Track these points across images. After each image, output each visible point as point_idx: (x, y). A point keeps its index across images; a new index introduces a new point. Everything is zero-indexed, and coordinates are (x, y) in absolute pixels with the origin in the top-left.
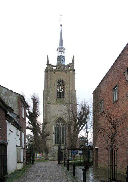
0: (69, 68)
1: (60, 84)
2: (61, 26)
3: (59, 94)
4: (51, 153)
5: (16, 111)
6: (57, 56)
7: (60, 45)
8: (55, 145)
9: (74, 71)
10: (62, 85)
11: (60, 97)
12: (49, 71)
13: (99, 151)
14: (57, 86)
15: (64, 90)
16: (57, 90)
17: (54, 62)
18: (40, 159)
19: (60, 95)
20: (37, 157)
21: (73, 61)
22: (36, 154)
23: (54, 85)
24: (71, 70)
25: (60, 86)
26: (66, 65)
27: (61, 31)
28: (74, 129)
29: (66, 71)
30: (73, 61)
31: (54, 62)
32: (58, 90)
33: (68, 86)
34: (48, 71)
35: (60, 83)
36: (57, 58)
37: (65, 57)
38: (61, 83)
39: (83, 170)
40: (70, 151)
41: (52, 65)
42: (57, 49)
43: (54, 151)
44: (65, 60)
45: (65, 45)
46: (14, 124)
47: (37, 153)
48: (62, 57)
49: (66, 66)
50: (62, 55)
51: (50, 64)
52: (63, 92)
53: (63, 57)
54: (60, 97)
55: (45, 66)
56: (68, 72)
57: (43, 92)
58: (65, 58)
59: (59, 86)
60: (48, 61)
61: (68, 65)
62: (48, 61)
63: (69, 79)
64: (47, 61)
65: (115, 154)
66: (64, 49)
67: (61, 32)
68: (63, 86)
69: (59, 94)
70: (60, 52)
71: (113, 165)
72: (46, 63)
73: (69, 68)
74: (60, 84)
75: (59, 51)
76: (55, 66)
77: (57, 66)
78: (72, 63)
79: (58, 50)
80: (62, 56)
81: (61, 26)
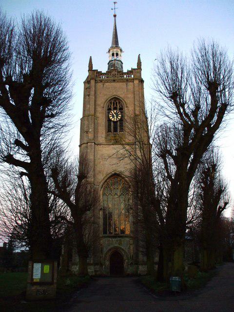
0: (132, 76)
2: (115, 16)
3: (112, 124)
7: (113, 44)
8: (104, 235)
9: (142, 81)
11: (115, 130)
12: (93, 82)
17: (103, 68)
18: (45, 288)
19: (115, 129)
20: (32, 279)
21: (139, 64)
24: (136, 79)
25: (115, 108)
26: (126, 71)
29: (127, 80)
30: (139, 64)
31: (103, 68)
35: (114, 103)
37: (123, 50)
38: (116, 103)
40: (93, 270)
48: (117, 62)
49: (125, 73)
54: (115, 130)
55: (87, 74)
56: (131, 83)
57: (80, 121)
59: (112, 108)
61: (130, 72)
63: (133, 96)
66: (121, 50)
67: (116, 25)
68: (121, 109)
69: (112, 124)
70: (113, 55)
73: (132, 76)
75: (111, 53)
76: (104, 74)
77: (108, 72)
79: (109, 51)
80: (117, 60)
81: (115, 16)
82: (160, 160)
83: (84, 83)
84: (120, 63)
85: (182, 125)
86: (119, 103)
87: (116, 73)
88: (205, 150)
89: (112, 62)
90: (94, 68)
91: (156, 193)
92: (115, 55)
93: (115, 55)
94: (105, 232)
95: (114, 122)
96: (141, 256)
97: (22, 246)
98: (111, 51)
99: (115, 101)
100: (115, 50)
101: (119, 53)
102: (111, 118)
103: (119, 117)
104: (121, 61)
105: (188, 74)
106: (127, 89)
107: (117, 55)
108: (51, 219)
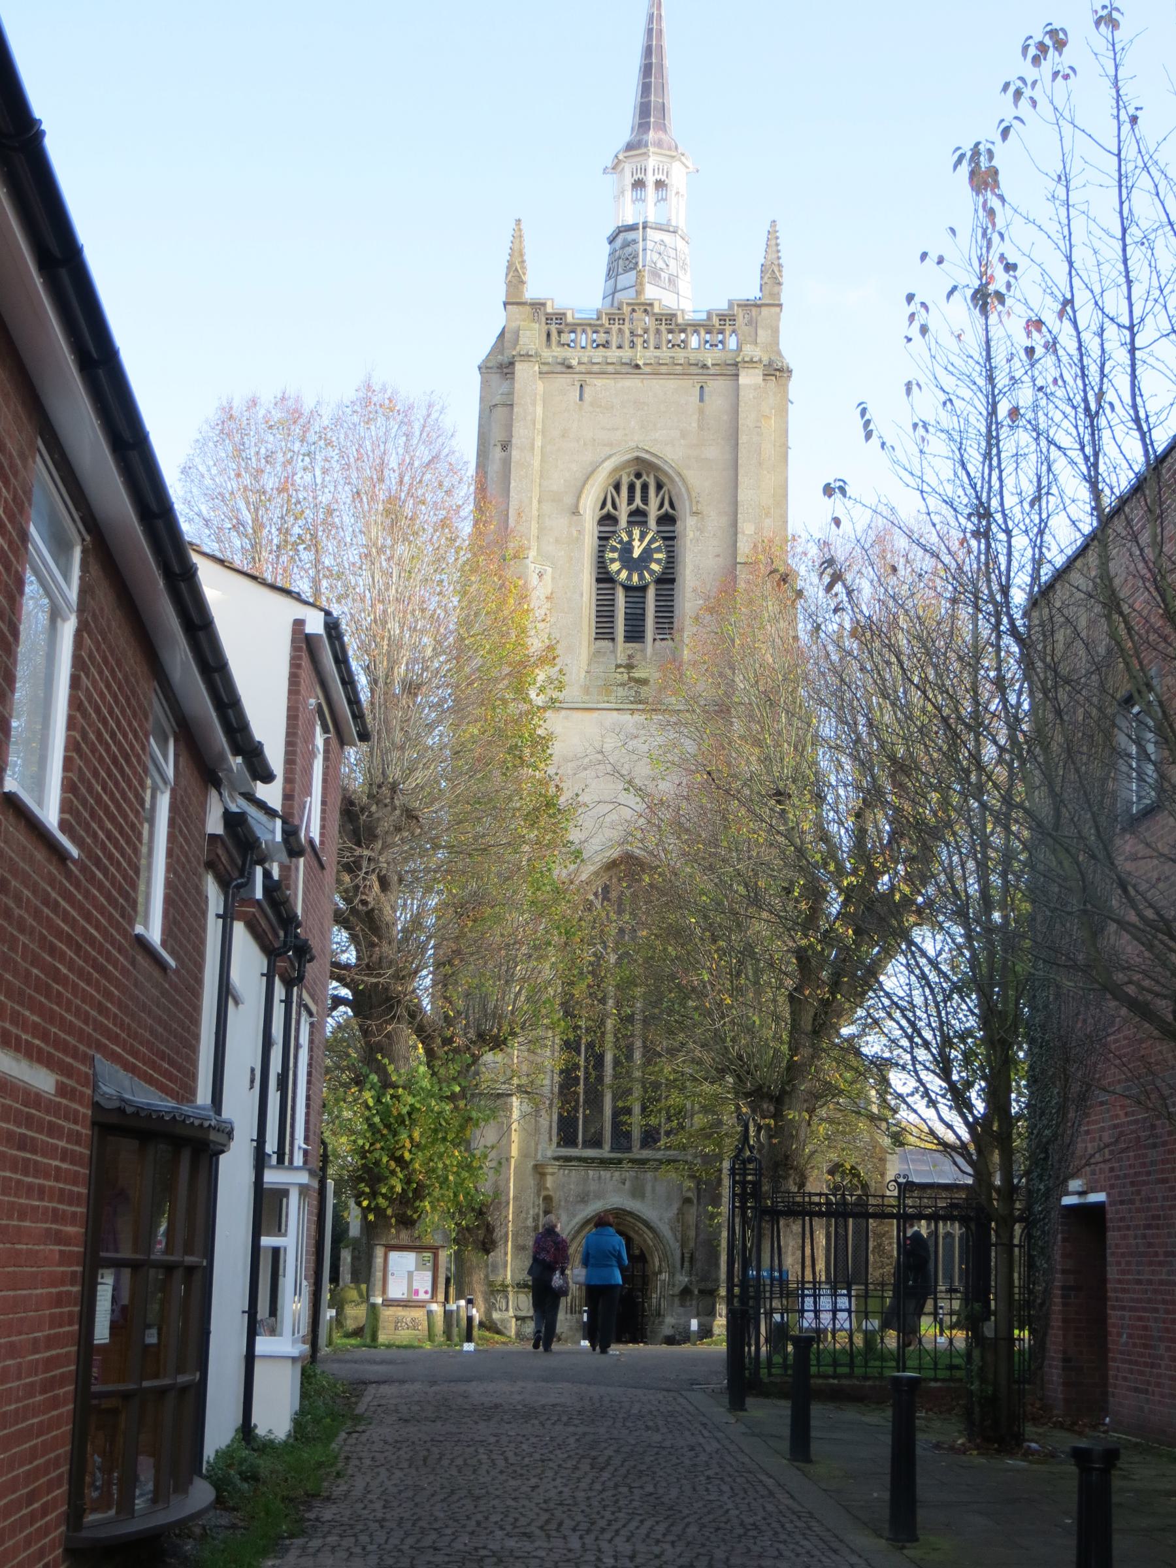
1: (638, 501)
3: (620, 595)
5: (730, 1122)
6: (610, 230)
10: (653, 512)
11: (635, 634)
13: (1112, 1237)
14: (607, 520)
15: (671, 562)
16: (601, 563)
21: (771, 274)
22: (379, 1260)
23: (575, 512)
30: (771, 274)
32: (615, 567)
33: (715, 521)
34: (519, 367)
35: (631, 488)
36: (607, 248)
38: (645, 487)
41: (560, 317)
46: (1115, 902)
47: (391, 1247)
51: (538, 306)
52: (667, 580)
54: (635, 634)
60: (515, 277)
62: (515, 277)
64: (510, 266)
68: (667, 520)
70: (639, 184)
71: (220, 794)
72: (500, 293)
74: (638, 501)
75: (629, 181)
79: (616, 166)
83: (484, 369)
85: (858, 788)
90: (531, 292)
94: (281, 1160)
95: (628, 588)
102: (615, 567)
103: (655, 567)
105: (682, 1267)
108: (1013, 1111)
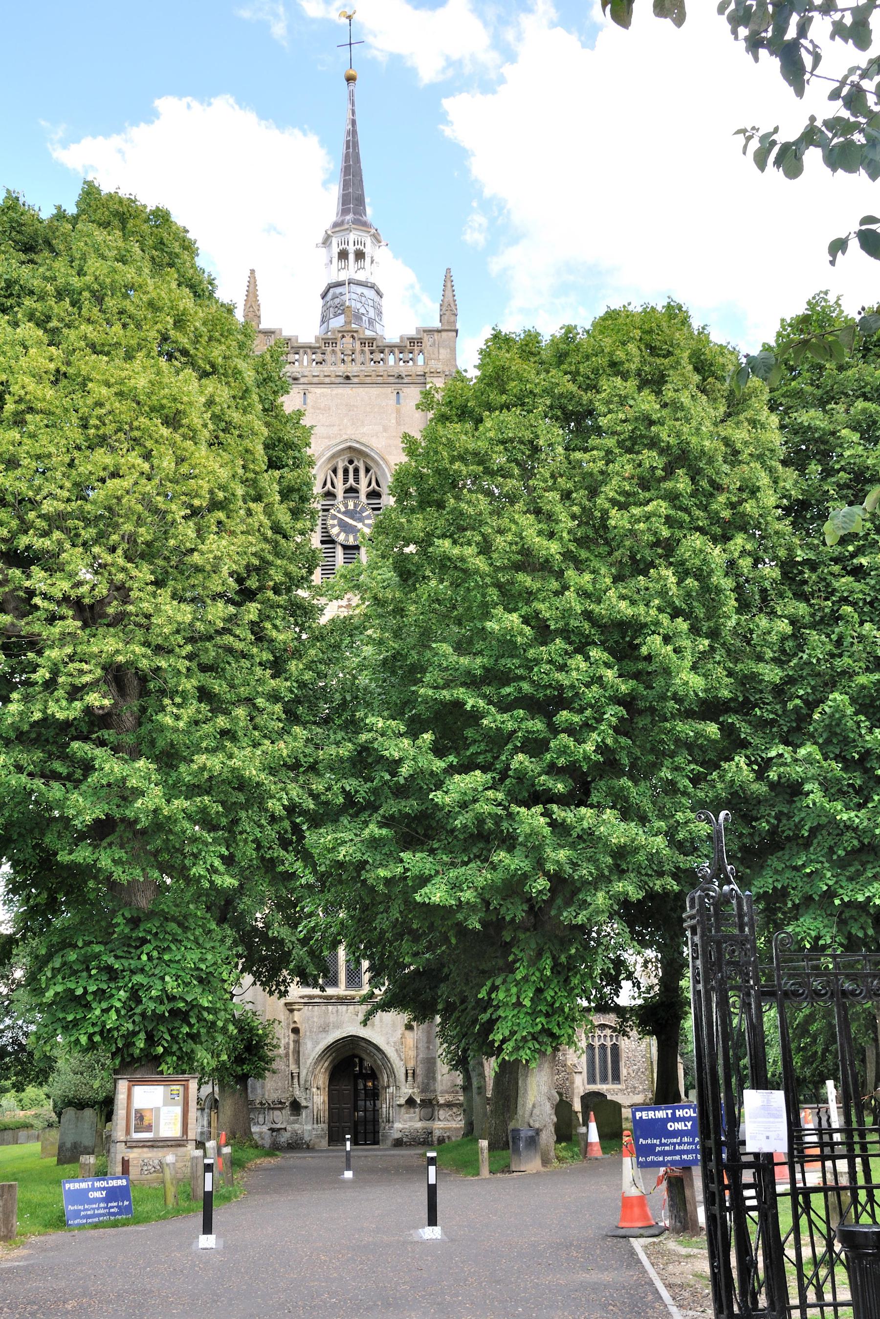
2: (350, 79)
4: (729, 978)
26: (396, 340)
27: (353, 132)
28: (478, 772)
30: (449, 310)
35: (346, 471)
37: (382, 290)
38: (356, 471)
39: (399, 762)
42: (320, 240)
43: (297, 1052)
44: (380, 313)
45: (357, 118)
48: (360, 290)
49: (392, 348)
50: (361, 276)
53: (366, 291)
58: (384, 302)
65: (859, 1168)
70: (343, 255)
75: (335, 250)
78: (437, 325)
79: (327, 241)
82: (761, 665)
84: (370, 293)
86: (367, 470)
87: (358, 345)
88: (511, 1118)
89: (338, 290)
91: (412, 968)
92: (351, 257)
93: (351, 257)
96: (181, 1203)
97: (411, 1119)
98: (335, 241)
99: (351, 462)
100: (352, 237)
101: (368, 250)
104: (372, 287)
106: (398, 411)
107: (360, 255)
